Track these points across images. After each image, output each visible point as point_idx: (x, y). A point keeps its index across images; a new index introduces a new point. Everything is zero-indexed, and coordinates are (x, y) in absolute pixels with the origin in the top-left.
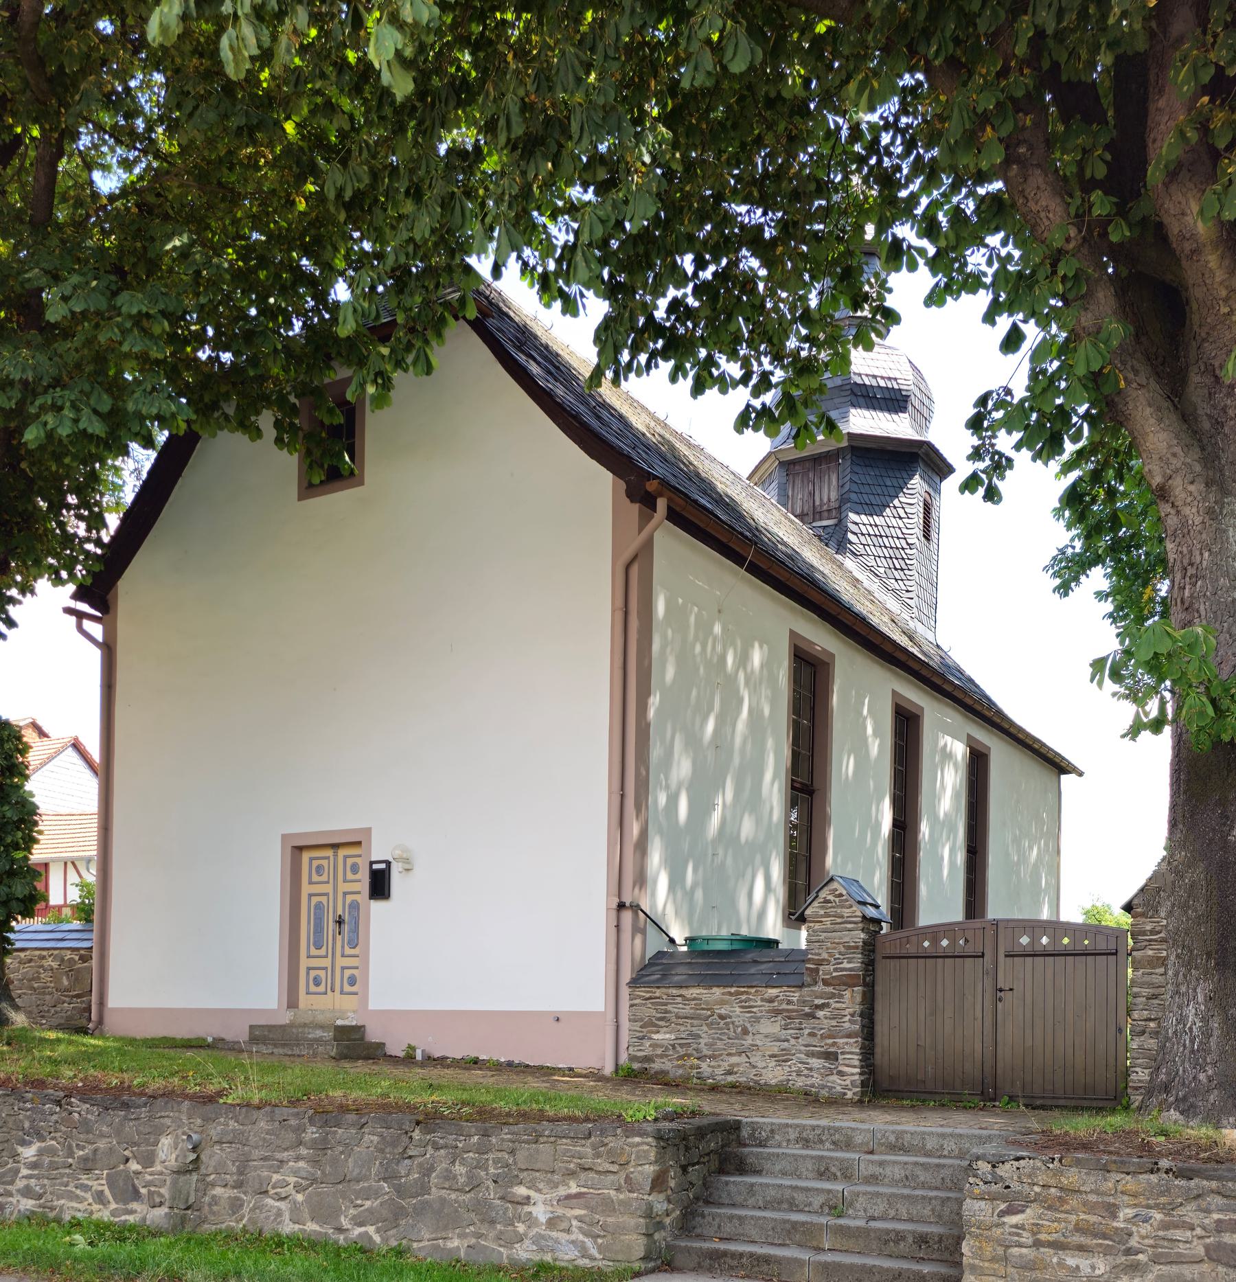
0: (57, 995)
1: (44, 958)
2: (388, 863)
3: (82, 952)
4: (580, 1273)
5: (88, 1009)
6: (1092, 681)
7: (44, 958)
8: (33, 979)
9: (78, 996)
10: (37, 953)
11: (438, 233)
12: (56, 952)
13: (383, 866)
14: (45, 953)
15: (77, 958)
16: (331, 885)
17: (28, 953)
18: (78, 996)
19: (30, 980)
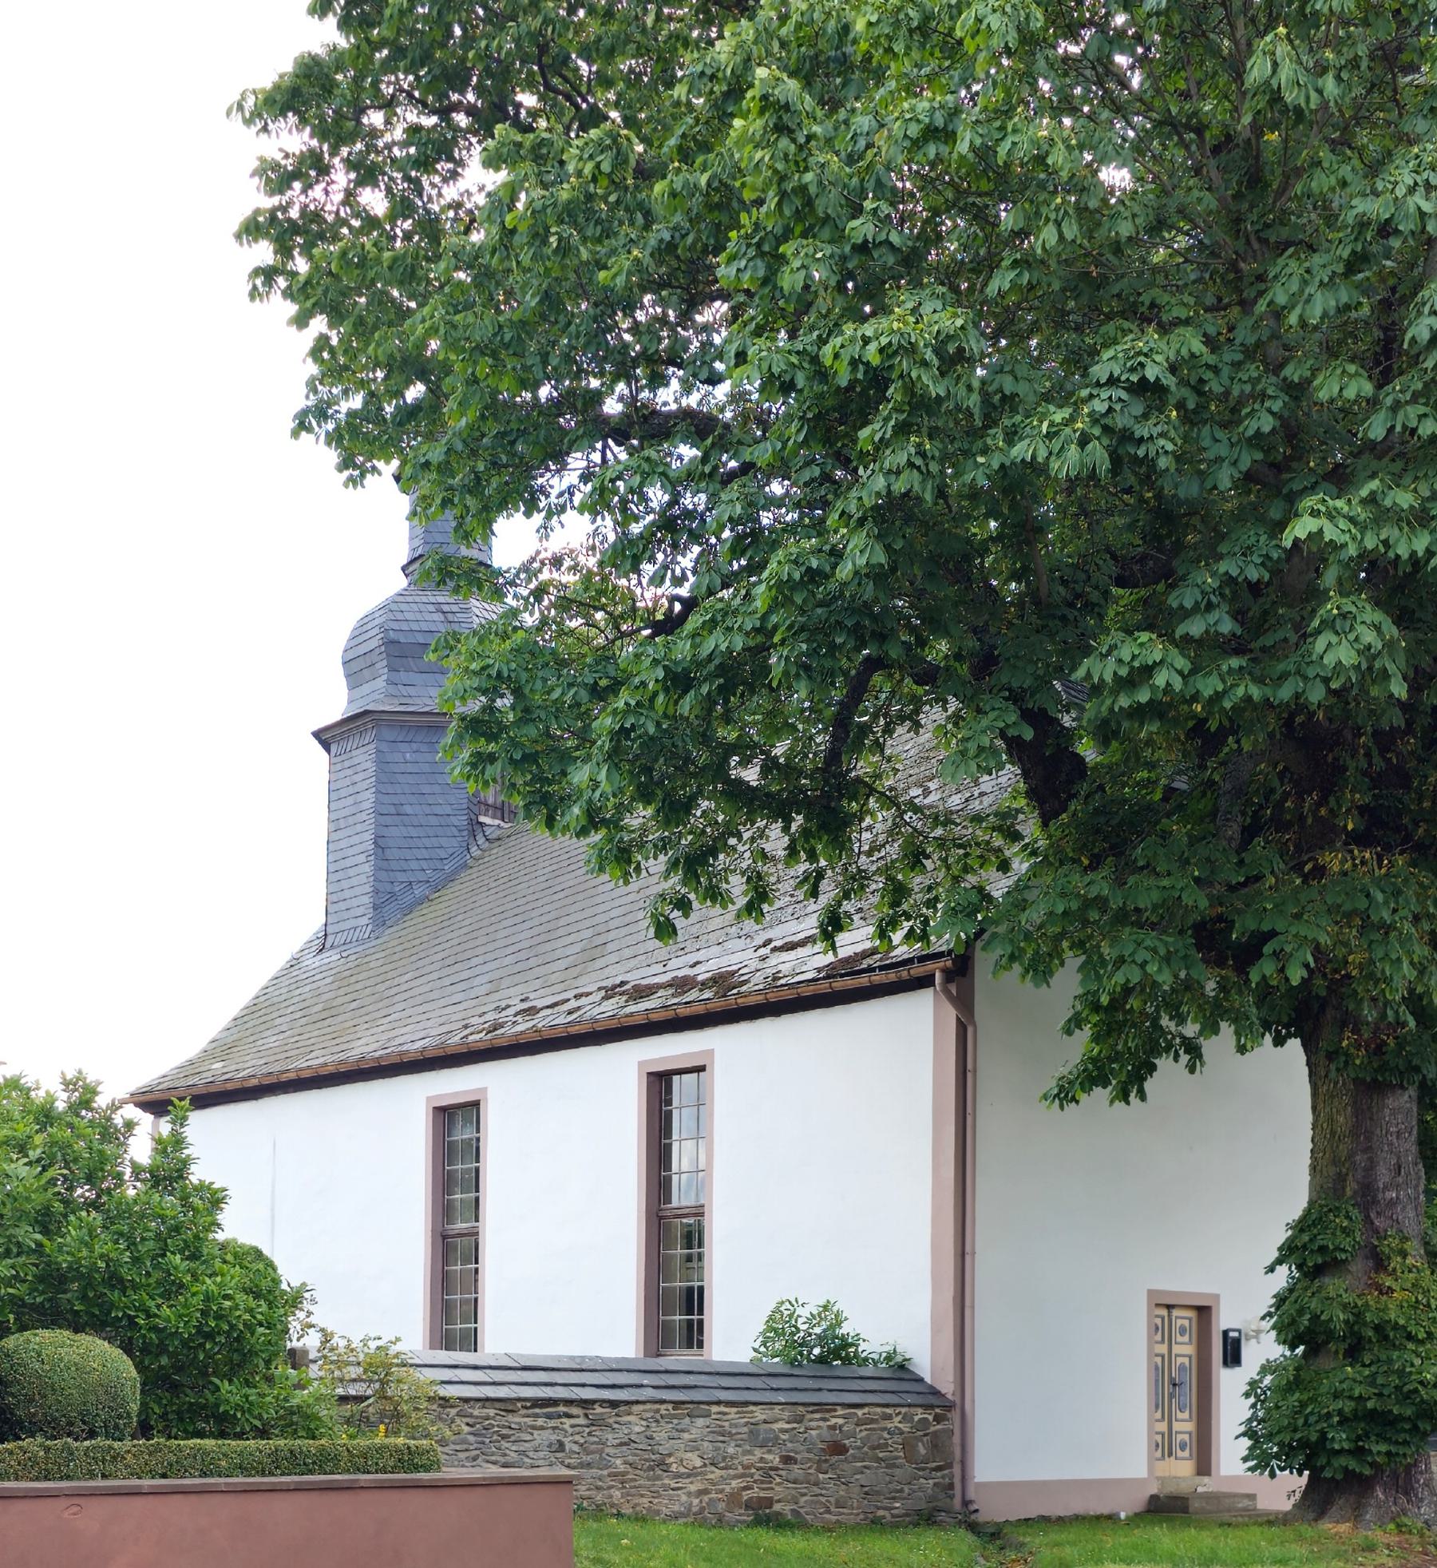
0: (909, 1468)
1: (889, 1417)
2: (1239, 1331)
3: (938, 1410)
4: (1407, 479)
5: (951, 1486)
6: (241, 244)
7: (889, 1417)
8: (879, 1447)
9: (939, 1469)
10: (878, 1410)
11: (596, 482)
12: (903, 1410)
13: (1236, 1334)
14: (889, 1411)
15: (931, 1418)
16: (1174, 1352)
17: (866, 1410)
18: (939, 1469)
19: (873, 1448)
